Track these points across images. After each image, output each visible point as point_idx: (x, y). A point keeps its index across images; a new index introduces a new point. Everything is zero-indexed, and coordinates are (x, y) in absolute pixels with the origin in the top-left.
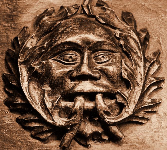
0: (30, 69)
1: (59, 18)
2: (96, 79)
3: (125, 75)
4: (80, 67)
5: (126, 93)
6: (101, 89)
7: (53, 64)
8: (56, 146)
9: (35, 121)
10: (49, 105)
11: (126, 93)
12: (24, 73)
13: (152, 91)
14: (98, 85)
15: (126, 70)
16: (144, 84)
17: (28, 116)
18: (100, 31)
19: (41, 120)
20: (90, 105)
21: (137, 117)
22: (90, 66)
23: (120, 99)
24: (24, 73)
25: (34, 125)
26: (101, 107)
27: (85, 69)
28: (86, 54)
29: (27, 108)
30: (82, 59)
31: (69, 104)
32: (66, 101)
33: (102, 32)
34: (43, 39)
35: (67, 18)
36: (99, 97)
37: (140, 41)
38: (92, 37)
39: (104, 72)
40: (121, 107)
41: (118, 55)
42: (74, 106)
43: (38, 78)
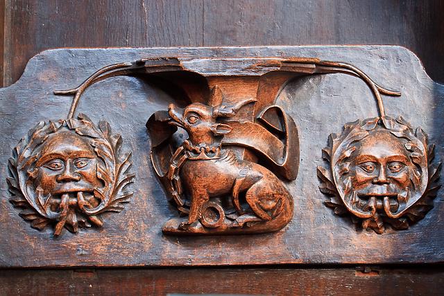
0: (27, 174)
1: (48, 132)
2: (76, 181)
3: (100, 176)
4: (63, 172)
5: (101, 190)
6: (82, 188)
7: (44, 170)
8: (363, 115)
9: (33, 215)
10: (42, 203)
11: (101, 190)
12: (21, 176)
13: (243, 106)
14: (80, 185)
15: (100, 172)
16: (117, 181)
17: (27, 212)
18: (79, 142)
19: (37, 214)
20: (74, 200)
21: (113, 208)
22: (71, 170)
23: (97, 195)
24: (21, 176)
25: (32, 218)
26: (82, 202)
27: (68, 174)
28: (68, 163)
29: (26, 205)
30: (65, 166)
31: (58, 201)
32: (56, 198)
33: (80, 143)
34: (36, 150)
35: (53, 132)
36: (80, 194)
37: (112, 146)
38: (74, 148)
39: (82, 175)
40: (99, 201)
41: (94, 160)
42: (61, 202)
43: (34, 182)
